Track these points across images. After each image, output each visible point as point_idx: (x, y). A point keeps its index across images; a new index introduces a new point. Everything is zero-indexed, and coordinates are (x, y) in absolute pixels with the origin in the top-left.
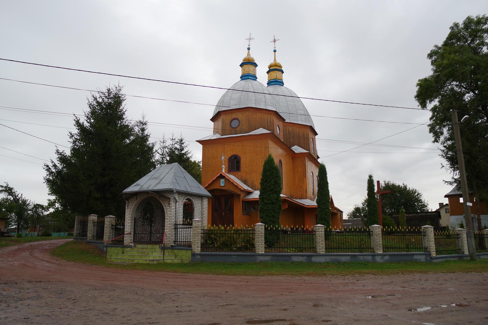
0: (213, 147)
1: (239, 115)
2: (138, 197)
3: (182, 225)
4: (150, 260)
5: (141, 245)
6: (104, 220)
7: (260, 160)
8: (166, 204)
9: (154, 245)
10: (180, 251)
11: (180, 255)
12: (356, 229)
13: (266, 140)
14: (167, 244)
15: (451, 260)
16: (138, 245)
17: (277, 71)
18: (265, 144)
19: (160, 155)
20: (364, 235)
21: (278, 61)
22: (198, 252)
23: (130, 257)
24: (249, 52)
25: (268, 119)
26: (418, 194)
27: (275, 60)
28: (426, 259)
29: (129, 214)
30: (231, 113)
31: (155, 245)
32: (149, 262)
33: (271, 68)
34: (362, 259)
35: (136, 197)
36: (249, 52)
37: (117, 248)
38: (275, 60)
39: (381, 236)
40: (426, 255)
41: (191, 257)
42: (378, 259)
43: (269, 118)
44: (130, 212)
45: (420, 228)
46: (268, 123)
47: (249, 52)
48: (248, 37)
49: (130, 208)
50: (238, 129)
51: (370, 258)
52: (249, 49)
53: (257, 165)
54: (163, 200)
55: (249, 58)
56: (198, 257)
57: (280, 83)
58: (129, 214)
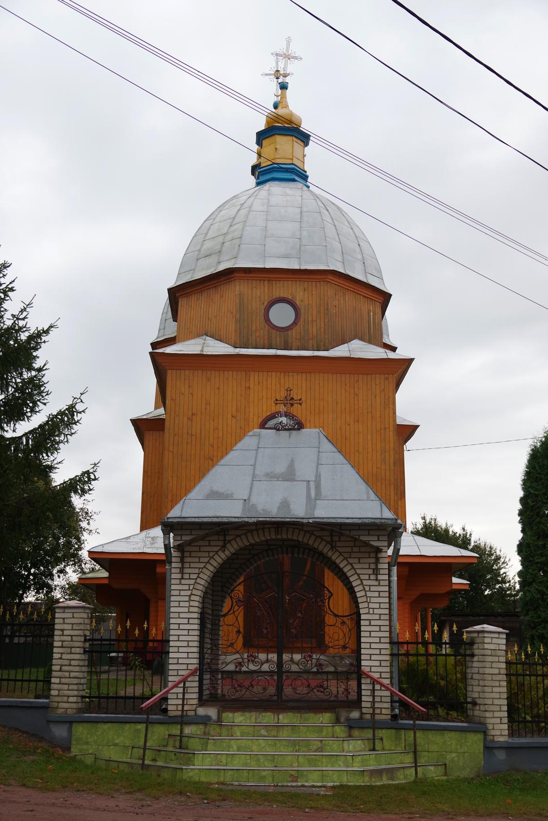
0: (209, 380)
1: (298, 291)
4: (372, 772)
5: (248, 715)
6: (54, 618)
7: (369, 437)
8: (359, 571)
9: (307, 715)
10: (431, 735)
11: (434, 748)
13: (386, 378)
16: (230, 715)
18: (384, 390)
22: (502, 739)
23: (258, 760)
25: (369, 316)
26: (498, 558)
29: (190, 600)
31: (311, 715)
32: (371, 777)
35: (222, 538)
37: (127, 726)
39: (505, 678)
41: (481, 755)
43: (372, 314)
44: (195, 592)
46: (369, 330)
48: (281, 47)
50: (294, 333)
53: (358, 451)
54: (346, 555)
56: (501, 755)
58: (190, 600)
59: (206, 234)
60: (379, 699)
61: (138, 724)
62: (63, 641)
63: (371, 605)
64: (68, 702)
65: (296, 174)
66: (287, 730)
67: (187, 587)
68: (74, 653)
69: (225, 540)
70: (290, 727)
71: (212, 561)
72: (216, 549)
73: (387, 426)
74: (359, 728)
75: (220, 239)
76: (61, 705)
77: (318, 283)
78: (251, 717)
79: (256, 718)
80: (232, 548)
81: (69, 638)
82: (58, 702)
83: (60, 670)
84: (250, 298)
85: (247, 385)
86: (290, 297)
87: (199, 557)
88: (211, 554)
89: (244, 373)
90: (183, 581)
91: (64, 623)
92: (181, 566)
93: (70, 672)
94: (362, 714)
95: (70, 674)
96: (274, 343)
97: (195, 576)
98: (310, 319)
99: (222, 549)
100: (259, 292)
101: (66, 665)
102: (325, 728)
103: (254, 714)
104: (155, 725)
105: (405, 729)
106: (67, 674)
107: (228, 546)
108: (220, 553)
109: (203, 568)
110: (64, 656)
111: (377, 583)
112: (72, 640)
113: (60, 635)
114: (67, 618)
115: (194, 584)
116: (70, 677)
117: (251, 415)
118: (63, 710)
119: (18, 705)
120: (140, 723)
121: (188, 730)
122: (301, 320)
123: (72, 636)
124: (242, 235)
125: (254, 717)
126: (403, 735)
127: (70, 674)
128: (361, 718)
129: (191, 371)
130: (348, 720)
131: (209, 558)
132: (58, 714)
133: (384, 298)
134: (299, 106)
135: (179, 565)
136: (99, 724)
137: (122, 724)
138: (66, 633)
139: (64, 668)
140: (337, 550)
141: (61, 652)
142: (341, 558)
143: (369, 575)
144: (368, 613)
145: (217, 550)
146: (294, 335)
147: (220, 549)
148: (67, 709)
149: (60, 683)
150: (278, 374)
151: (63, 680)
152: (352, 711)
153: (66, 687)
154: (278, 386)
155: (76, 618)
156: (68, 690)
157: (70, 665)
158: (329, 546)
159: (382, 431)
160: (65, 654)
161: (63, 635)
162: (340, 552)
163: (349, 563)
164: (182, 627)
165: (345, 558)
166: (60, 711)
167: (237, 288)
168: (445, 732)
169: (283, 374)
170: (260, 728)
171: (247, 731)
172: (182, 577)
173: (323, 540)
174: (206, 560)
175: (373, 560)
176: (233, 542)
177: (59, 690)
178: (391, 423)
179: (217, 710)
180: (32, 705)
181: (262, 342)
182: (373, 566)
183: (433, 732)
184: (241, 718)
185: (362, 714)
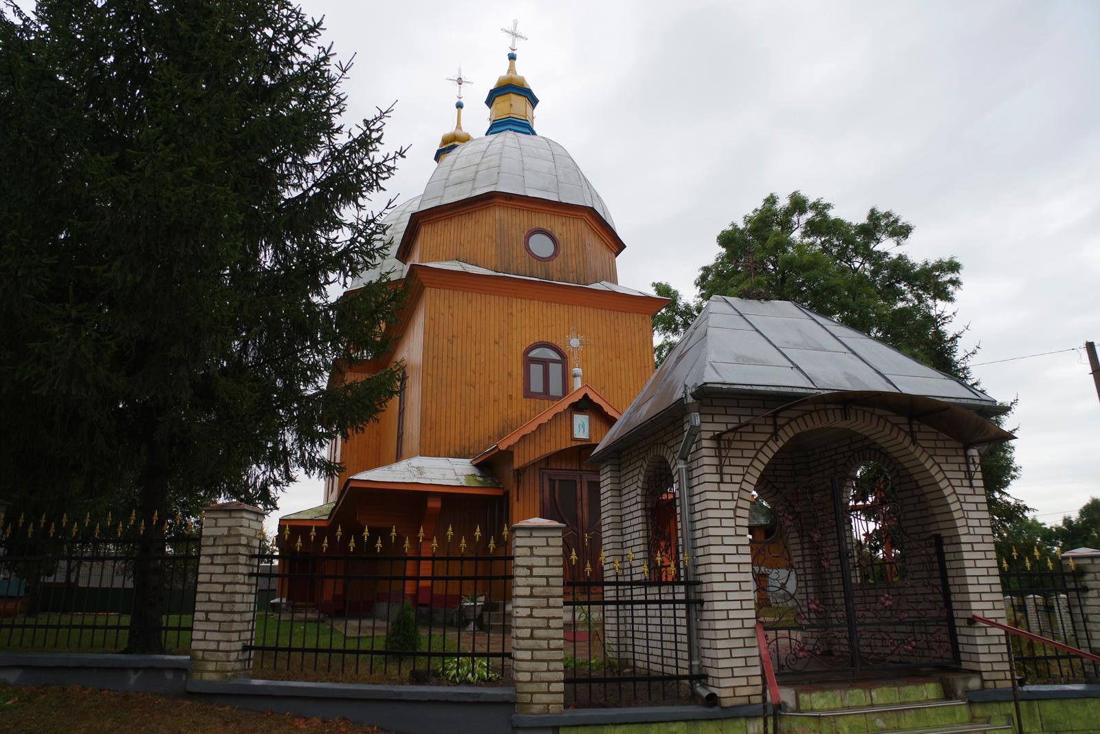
0: (471, 302)
1: (556, 225)
2: (780, 422)
3: (645, 584)
5: (830, 695)
7: (631, 374)
8: (949, 475)
14: (994, 676)
18: (642, 329)
20: (28, 626)
30: (530, 210)
44: (741, 503)
49: (738, 479)
50: (554, 265)
53: (621, 387)
54: (931, 452)
55: (511, 79)
59: (453, 165)
60: (989, 653)
61: (670, 724)
62: (532, 587)
63: (971, 523)
64: (549, 692)
65: (525, 127)
66: (910, 717)
67: (729, 496)
68: (554, 607)
69: (775, 424)
70: (913, 711)
71: (760, 456)
72: (764, 437)
73: (647, 365)
74: (980, 703)
75: (474, 168)
76: (537, 698)
77: (575, 220)
78: (834, 697)
79: (842, 700)
80: (786, 436)
81: (544, 581)
82: (532, 693)
83: (532, 637)
84: (510, 225)
85: (510, 312)
86: (549, 229)
87: (742, 450)
88: (758, 446)
89: (506, 298)
90: (723, 487)
91: (532, 555)
92: (717, 463)
93: (549, 639)
94: (983, 681)
95: (548, 644)
96: (535, 272)
97: (738, 479)
98: (569, 253)
99: (774, 438)
100: (518, 221)
101: (540, 628)
102: (957, 708)
103: (837, 692)
104: (700, 723)
105: (1038, 700)
106: (544, 644)
107: (781, 433)
108: (771, 443)
109: (748, 467)
110: (536, 613)
111: (970, 491)
112: (548, 585)
113: (526, 577)
114: (537, 547)
115: (739, 492)
116: (549, 649)
117: (515, 342)
118: (541, 707)
119: (450, 699)
120: (674, 721)
121: (754, 728)
122: (561, 252)
123: (547, 577)
124: (444, 190)
125: (839, 699)
126: (1037, 708)
127: (548, 644)
128: (983, 687)
129: (452, 291)
130: (967, 691)
131: (755, 452)
132: (534, 714)
133: (619, 246)
134: (526, 72)
135: (715, 461)
136: (606, 727)
137: (645, 725)
138: (536, 571)
139: (537, 633)
140: (919, 445)
141: (530, 604)
142: (925, 456)
143: (961, 479)
144: (969, 534)
145: (765, 439)
146: (555, 267)
147: (771, 438)
148: (548, 704)
149: (532, 660)
150: (541, 303)
151: (538, 655)
152: (969, 678)
153: (544, 666)
154: (541, 315)
155: (553, 546)
156: (548, 671)
157: (548, 627)
158: (908, 439)
159: (643, 369)
160: (537, 608)
161: (531, 576)
162: (923, 448)
163: (936, 463)
164: (728, 559)
165: (931, 456)
166: (536, 709)
167: (498, 215)
168: (1087, 700)
169: (545, 304)
170: (873, 717)
171: (857, 724)
172: (722, 479)
173: (900, 429)
174: (752, 454)
175: (962, 460)
176: (787, 428)
177: (532, 672)
178: (650, 361)
179: (793, 692)
180: (402, 698)
181: (523, 270)
182: (964, 468)
183: (1072, 701)
184: (822, 702)
185: (983, 681)
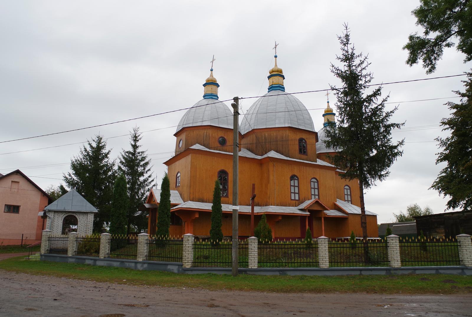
12: (439, 239)
15: (200, 274)
17: (273, 77)
19: (442, 125)
21: (279, 67)
24: (212, 73)
25: (204, 134)
27: (276, 65)
28: (179, 271)
33: (274, 73)
34: (127, 265)
36: (212, 73)
38: (276, 65)
40: (179, 265)
42: (139, 266)
43: (205, 133)
45: (311, 240)
47: (212, 73)
51: (133, 265)
52: (212, 70)
57: (281, 88)
